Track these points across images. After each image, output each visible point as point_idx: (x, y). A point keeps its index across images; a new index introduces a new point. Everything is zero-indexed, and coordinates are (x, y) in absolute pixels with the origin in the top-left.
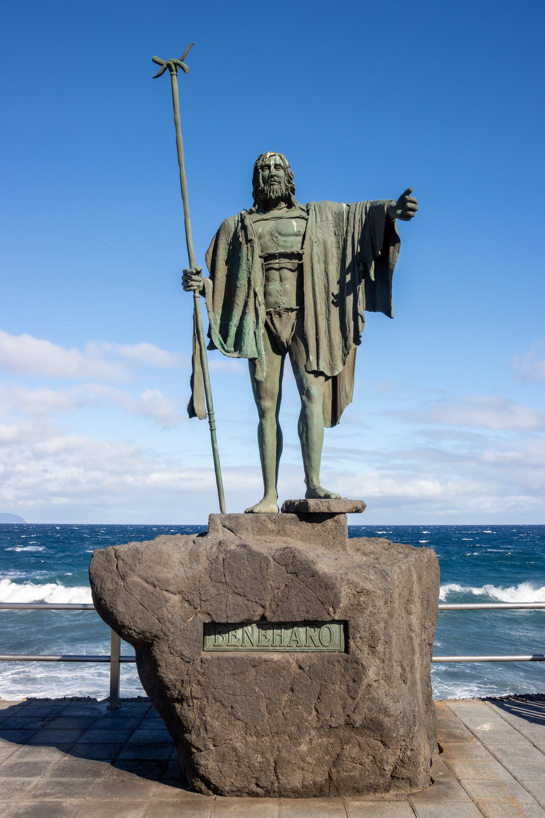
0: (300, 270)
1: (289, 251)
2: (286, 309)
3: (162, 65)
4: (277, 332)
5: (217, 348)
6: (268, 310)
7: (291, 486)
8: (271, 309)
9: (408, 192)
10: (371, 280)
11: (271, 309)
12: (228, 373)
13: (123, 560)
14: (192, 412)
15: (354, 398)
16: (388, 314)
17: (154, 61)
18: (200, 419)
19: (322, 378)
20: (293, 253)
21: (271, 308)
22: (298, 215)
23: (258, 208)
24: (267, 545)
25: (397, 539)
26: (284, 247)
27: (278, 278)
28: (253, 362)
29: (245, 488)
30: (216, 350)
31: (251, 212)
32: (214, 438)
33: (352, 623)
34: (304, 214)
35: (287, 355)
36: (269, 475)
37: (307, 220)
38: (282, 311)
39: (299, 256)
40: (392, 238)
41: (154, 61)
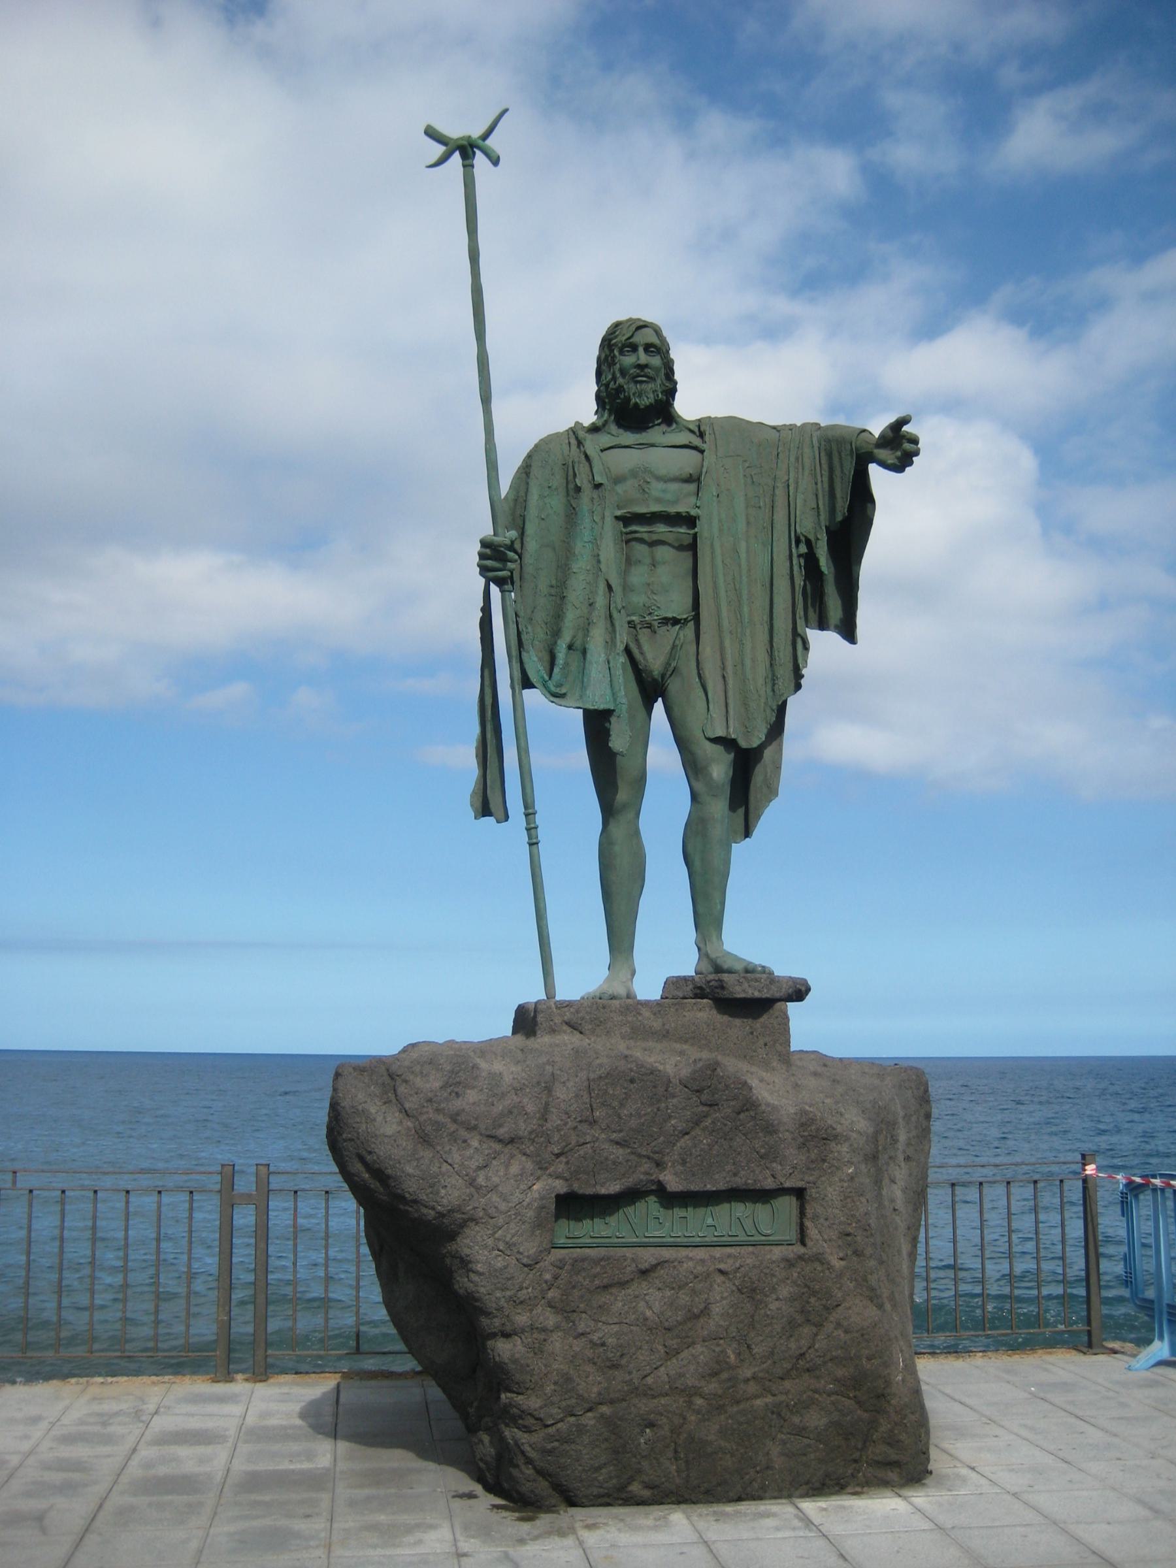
0: (692, 547)
1: (672, 510)
2: (665, 618)
4: (645, 659)
5: (534, 687)
7: (666, 951)
9: (904, 421)
11: (634, 618)
14: (484, 808)
15: (782, 789)
17: (506, 111)
20: (678, 514)
21: (633, 614)
22: (685, 442)
24: (672, 1062)
25: (801, 1059)
26: (659, 500)
27: (648, 560)
32: (536, 858)
33: (812, 1192)
34: (696, 441)
35: (659, 706)
37: (702, 452)
38: (656, 624)
39: (690, 521)
40: (862, 501)
41: (506, 111)
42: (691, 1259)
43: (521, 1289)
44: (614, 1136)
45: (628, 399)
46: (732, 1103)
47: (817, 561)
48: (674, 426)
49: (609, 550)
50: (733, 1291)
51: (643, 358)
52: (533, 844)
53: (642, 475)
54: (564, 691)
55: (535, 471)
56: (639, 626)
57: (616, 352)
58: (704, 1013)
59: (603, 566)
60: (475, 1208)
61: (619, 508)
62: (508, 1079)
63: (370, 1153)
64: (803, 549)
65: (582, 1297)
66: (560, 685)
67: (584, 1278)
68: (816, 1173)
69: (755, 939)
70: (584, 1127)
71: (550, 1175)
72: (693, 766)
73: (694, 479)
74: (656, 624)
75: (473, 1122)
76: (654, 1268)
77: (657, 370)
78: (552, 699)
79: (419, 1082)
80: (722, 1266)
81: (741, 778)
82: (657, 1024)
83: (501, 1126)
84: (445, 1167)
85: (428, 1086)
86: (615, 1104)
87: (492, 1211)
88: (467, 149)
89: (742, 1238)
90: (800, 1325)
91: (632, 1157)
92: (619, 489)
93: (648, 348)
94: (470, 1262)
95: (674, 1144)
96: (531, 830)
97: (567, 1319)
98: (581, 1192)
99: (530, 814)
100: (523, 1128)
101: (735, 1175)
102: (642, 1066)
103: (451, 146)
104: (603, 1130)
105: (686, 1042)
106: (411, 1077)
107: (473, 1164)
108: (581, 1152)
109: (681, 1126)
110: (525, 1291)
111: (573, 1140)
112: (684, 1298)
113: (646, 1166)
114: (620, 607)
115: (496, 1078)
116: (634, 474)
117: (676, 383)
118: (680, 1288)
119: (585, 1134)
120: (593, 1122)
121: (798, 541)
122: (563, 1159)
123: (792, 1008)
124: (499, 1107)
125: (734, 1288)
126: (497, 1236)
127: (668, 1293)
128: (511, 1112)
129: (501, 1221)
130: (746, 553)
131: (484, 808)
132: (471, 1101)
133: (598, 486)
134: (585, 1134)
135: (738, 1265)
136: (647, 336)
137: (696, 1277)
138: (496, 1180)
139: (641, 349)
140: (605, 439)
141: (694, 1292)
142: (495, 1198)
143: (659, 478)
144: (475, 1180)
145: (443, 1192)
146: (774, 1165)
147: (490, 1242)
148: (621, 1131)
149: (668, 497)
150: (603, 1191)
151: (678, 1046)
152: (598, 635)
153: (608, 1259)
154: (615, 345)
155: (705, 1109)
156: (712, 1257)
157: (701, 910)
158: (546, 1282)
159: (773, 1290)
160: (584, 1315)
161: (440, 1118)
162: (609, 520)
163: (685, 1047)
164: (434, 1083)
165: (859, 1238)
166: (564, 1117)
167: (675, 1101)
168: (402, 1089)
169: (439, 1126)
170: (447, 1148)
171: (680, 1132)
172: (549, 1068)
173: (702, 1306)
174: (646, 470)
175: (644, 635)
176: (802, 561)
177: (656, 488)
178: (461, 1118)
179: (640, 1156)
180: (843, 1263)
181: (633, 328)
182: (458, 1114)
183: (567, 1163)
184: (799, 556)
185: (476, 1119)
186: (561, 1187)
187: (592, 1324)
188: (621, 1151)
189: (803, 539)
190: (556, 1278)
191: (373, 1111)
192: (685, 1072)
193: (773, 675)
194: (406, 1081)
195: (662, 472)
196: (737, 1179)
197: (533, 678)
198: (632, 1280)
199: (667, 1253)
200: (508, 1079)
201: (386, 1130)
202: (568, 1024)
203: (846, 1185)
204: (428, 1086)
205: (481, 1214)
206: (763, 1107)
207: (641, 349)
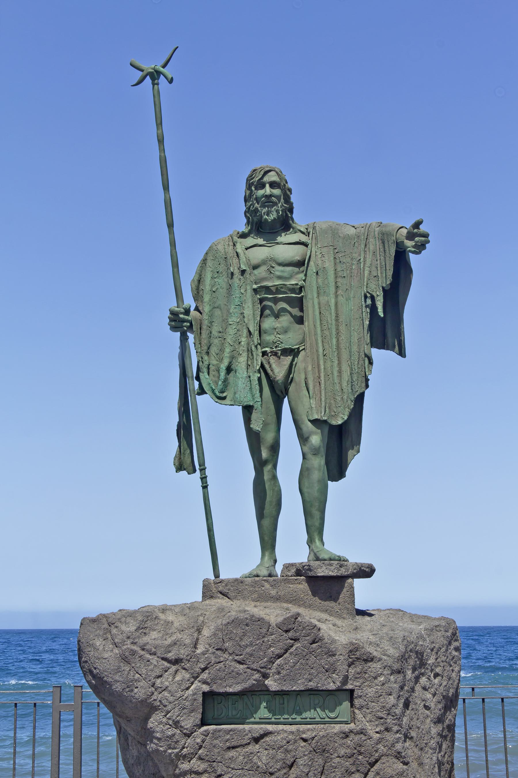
3: (142, 71)
4: (273, 373)
6: (264, 350)
8: (267, 349)
10: (379, 316)
11: (267, 349)
12: (221, 426)
13: (352, 732)
14: (180, 468)
16: (402, 353)
18: (189, 474)
19: (349, 357)
21: (267, 347)
23: (252, 228)
24: (274, 614)
28: (248, 410)
29: (242, 559)
30: (205, 395)
31: (243, 236)
36: (268, 542)
41: (131, 65)
42: (286, 732)
43: (183, 748)
44: (236, 658)
45: (262, 217)
46: (307, 638)
47: (377, 308)
48: (291, 230)
49: (250, 310)
50: (311, 751)
51: (268, 190)
52: (205, 487)
53: (271, 263)
54: (224, 395)
55: (209, 263)
56: (270, 354)
57: (253, 188)
58: (302, 587)
59: (246, 320)
60: (155, 700)
61: (256, 283)
62: (176, 624)
63: (95, 668)
64: (369, 302)
65: (219, 753)
66: (222, 392)
67: (220, 741)
68: (361, 681)
69: (342, 542)
70: (219, 653)
71: (200, 681)
72: (303, 438)
73: (300, 264)
74: (280, 352)
75: (154, 650)
76: (262, 736)
77: (278, 197)
78: (217, 400)
79: (123, 627)
80: (304, 736)
81: (339, 444)
82: (273, 592)
83: (170, 652)
84: (137, 676)
85: (128, 629)
86: (237, 639)
87: (164, 702)
88: (155, 76)
89: (318, 719)
90: (353, 773)
91: (248, 670)
92: (256, 272)
93: (273, 185)
94: (154, 732)
95: (274, 663)
96: (204, 479)
97: (211, 766)
98: (217, 691)
99: (203, 470)
100: (183, 653)
101: (310, 681)
102: (253, 616)
103: (145, 73)
104: (230, 654)
105: (290, 603)
106: (120, 624)
107: (154, 674)
108: (217, 667)
109: (277, 652)
110: (185, 750)
111: (213, 660)
112: (280, 755)
113: (257, 676)
114: (256, 343)
115: (168, 624)
116: (264, 262)
117: (292, 204)
118: (279, 748)
119: (220, 657)
120: (223, 650)
121: (366, 297)
122: (207, 671)
123: (358, 583)
124: (169, 641)
125: (312, 749)
126: (168, 716)
127: (271, 752)
128: (175, 644)
129: (169, 707)
130: (340, 305)
131: (180, 468)
132: (153, 637)
133: (243, 272)
134: (220, 657)
135: (313, 735)
136: (272, 177)
137: (288, 742)
138: (167, 683)
139: (267, 186)
140: (250, 241)
141: (287, 751)
142: (166, 694)
143: (280, 264)
144: (154, 684)
145: (136, 690)
146: (334, 675)
147: (164, 720)
148: (241, 655)
149: (285, 275)
150: (231, 690)
151: (285, 605)
152: (243, 359)
153: (235, 730)
154: (253, 184)
155: (292, 642)
156: (298, 730)
157: (309, 523)
158: (198, 744)
159: (335, 750)
160: (220, 764)
161: (135, 648)
162: (249, 292)
163: (290, 605)
164: (130, 627)
165: (388, 721)
166: (207, 646)
167: (273, 637)
168: (114, 631)
169: (133, 653)
170: (138, 665)
171: (277, 655)
172: (201, 618)
173: (292, 760)
174: (272, 259)
175: (273, 360)
176: (368, 310)
177: (279, 270)
178: (147, 647)
179: (252, 669)
180: (378, 735)
181: (262, 173)
182: (145, 645)
183: (209, 673)
184: (367, 306)
185: (155, 648)
186: (206, 688)
187: (225, 769)
188: (242, 666)
189: (368, 295)
190: (203, 741)
191: (98, 645)
192: (280, 619)
193: (352, 379)
194: (117, 627)
195: (281, 259)
196: (311, 683)
197: (206, 388)
198: (249, 744)
199: (270, 728)
200: (176, 624)
201: (105, 655)
202: (221, 593)
203: (379, 688)
204: (128, 629)
205: (159, 704)
206: (326, 640)
207: (267, 186)
